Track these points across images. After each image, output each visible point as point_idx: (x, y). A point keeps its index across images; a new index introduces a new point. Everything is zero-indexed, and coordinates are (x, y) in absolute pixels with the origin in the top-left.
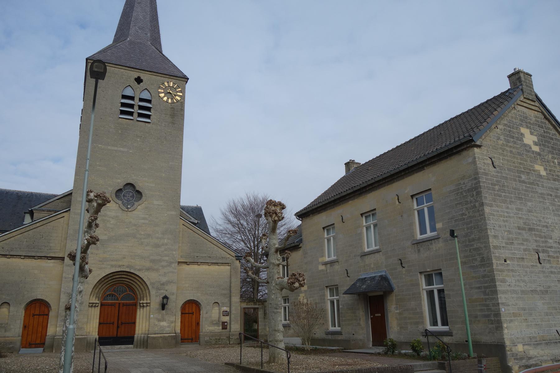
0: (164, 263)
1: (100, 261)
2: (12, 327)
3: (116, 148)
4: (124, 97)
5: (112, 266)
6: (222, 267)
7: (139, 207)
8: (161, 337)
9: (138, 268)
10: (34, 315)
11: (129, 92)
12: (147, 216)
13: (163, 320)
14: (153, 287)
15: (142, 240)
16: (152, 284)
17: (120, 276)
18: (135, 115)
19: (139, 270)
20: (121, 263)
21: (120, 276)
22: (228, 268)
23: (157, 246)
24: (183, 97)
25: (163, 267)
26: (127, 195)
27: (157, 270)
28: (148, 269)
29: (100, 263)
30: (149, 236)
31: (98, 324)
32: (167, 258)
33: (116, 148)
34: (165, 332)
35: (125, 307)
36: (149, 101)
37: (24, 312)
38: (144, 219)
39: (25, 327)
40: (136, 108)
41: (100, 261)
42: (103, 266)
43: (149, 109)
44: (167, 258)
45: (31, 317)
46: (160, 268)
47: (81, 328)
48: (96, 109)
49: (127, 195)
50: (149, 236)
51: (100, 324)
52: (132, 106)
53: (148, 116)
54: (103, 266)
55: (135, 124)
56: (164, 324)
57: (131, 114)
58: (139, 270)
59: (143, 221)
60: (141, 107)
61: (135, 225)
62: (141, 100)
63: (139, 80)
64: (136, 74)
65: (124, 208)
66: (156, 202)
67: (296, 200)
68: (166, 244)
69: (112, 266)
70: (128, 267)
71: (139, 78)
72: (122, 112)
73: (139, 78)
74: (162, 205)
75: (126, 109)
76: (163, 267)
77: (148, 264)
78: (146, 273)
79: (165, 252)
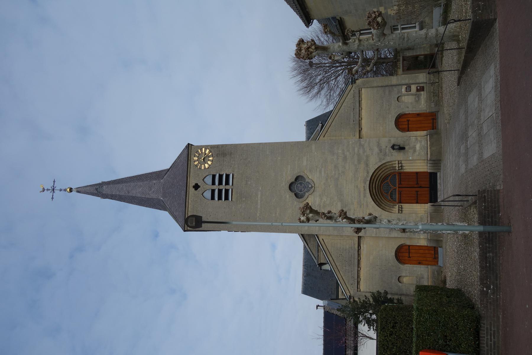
0: (361, 152)
1: (361, 207)
2: (419, 273)
3: (259, 201)
4: (213, 198)
5: (365, 196)
6: (363, 96)
7: (310, 177)
8: (430, 148)
9: (366, 174)
10: (409, 257)
11: (208, 194)
12: (318, 170)
16: (380, 161)
17: (374, 189)
18: (227, 187)
19: (368, 173)
20: (362, 189)
21: (374, 189)
22: (363, 90)
23: (345, 159)
24: (206, 147)
25: (364, 151)
27: (367, 157)
28: (367, 165)
29: (362, 206)
30: (335, 167)
31: (418, 205)
32: (356, 149)
33: (259, 201)
35: (402, 183)
36: (214, 177)
38: (320, 172)
39: (420, 263)
40: (221, 187)
41: (361, 207)
42: (365, 204)
43: (221, 176)
44: (356, 149)
46: (365, 154)
47: (421, 218)
52: (220, 191)
53: (227, 176)
54: (365, 204)
55: (236, 186)
56: (418, 147)
57: (227, 191)
58: (368, 173)
59: (323, 173)
60: (220, 183)
61: (327, 180)
62: (213, 183)
63: (196, 187)
64: (192, 190)
65: (312, 190)
66: (305, 163)
69: (365, 196)
71: (194, 187)
72: (227, 198)
73: (194, 187)
76: (364, 151)
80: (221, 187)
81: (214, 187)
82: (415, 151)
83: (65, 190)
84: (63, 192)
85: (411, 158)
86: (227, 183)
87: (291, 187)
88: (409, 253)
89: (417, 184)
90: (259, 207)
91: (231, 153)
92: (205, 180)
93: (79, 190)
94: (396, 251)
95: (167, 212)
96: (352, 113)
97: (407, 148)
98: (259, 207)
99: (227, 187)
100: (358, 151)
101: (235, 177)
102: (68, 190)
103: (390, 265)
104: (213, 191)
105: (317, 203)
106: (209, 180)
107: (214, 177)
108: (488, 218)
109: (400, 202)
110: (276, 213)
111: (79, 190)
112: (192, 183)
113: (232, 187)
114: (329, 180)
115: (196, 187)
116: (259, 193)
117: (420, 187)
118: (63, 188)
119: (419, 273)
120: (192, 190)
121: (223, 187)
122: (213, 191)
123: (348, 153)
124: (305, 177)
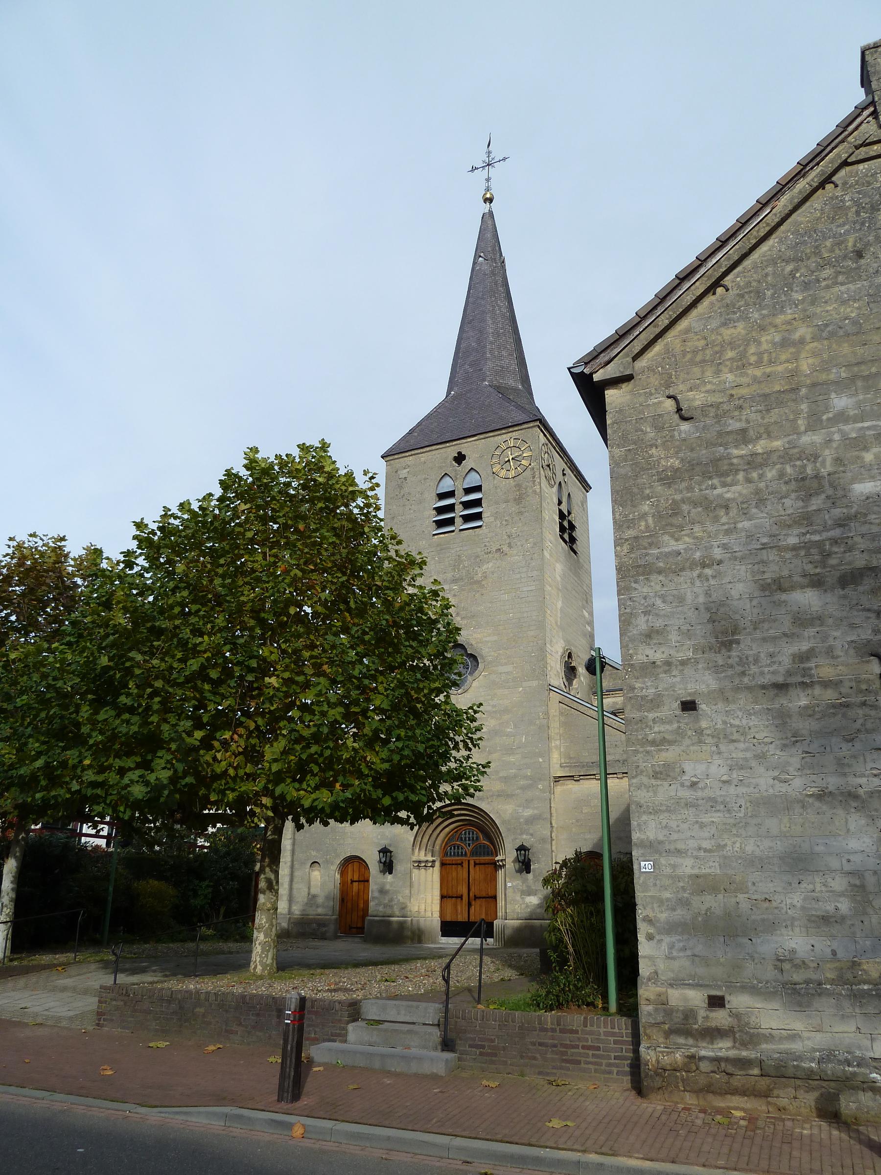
7: (475, 684)
11: (447, 485)
18: (458, 521)
21: (459, 812)
35: (477, 867)
40: (459, 508)
43: (478, 503)
51: (443, 897)
57: (451, 522)
60: (467, 505)
64: (451, 451)
71: (460, 453)
73: (460, 453)
80: (459, 508)
81: (459, 492)
83: (488, 189)
84: (484, 185)
85: (509, 884)
86: (467, 519)
88: (359, 881)
89: (476, 898)
93: (488, 219)
95: (538, 403)
99: (458, 521)
102: (488, 196)
104: (451, 494)
106: (473, 480)
107: (478, 489)
108: (601, 1065)
109: (443, 864)
111: (488, 219)
112: (465, 447)
113: (457, 530)
115: (460, 458)
117: (470, 905)
118: (492, 184)
120: (451, 451)
121: (460, 511)
122: (451, 494)
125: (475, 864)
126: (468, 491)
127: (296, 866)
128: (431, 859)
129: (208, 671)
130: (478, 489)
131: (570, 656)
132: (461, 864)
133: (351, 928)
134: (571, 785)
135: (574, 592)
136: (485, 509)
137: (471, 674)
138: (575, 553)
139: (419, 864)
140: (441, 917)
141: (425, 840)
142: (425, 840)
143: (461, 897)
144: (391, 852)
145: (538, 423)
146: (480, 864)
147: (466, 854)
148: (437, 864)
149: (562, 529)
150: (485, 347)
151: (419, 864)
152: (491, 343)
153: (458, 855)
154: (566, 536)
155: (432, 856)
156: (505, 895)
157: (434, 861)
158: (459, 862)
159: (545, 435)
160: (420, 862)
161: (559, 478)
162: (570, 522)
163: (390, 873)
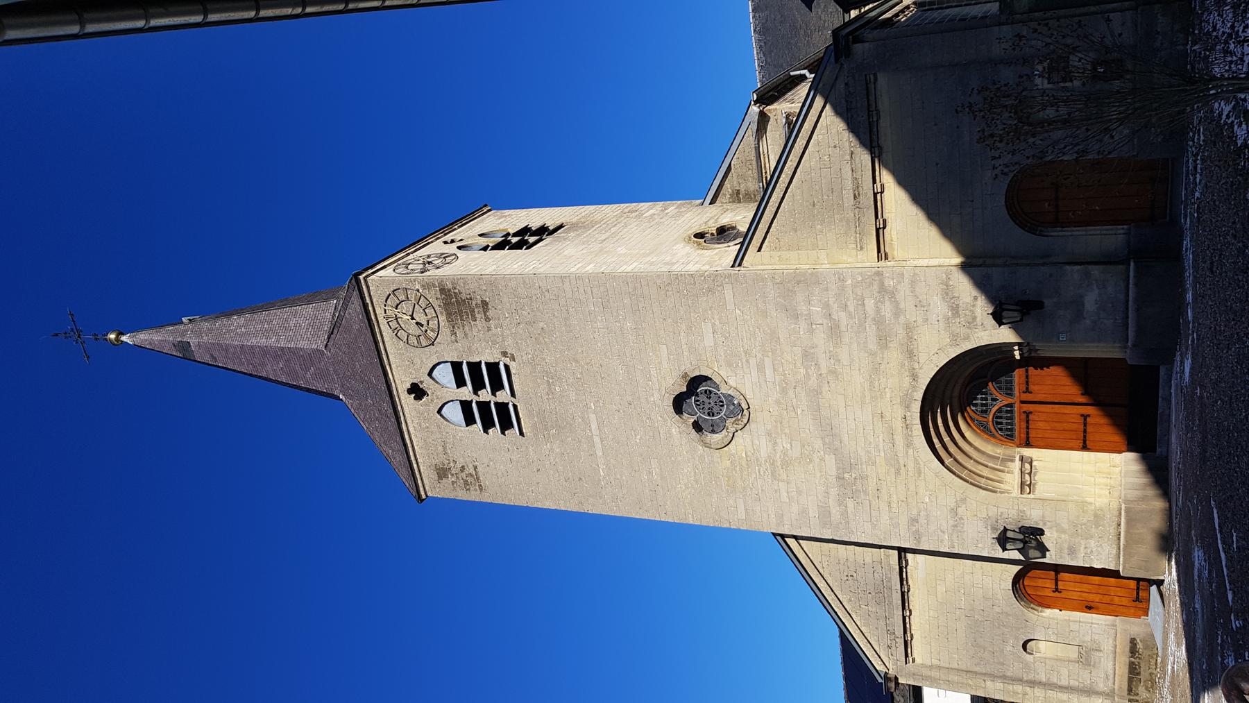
0: (887, 310)
1: (898, 472)
2: (1088, 638)
3: (597, 439)
5: (909, 444)
6: (884, 104)
7: (731, 382)
8: (1137, 310)
9: (907, 381)
10: (1057, 590)
12: (753, 361)
13: (1077, 305)
14: (967, 338)
15: (824, 371)
16: (955, 339)
19: (915, 377)
20: (899, 424)
22: (883, 81)
23: (834, 331)
25: (898, 312)
26: (707, 406)
27: (910, 328)
28: (911, 355)
29: (903, 471)
30: (808, 355)
31: (1086, 453)
32: (870, 303)
33: (597, 439)
34: (1122, 297)
35: (1032, 387)
37: (1048, 612)
38: (761, 368)
39: (1089, 608)
41: (898, 472)
42: (911, 465)
44: (870, 303)
45: (1063, 595)
46: (902, 319)
47: (1096, 516)
48: (558, 223)
49: (707, 406)
50: (808, 355)
51: (1085, 448)
54: (911, 465)
55: (525, 393)
56: (1091, 301)
58: (915, 377)
59: (769, 372)
61: (784, 391)
66: (709, 341)
67: (512, 231)
68: (827, 306)
69: (909, 444)
70: (908, 407)
71: (410, 391)
73: (410, 391)
74: (713, 325)
75: (500, 418)
76: (898, 312)
77: (894, 355)
78: (923, 358)
79: (851, 308)
82: (1079, 315)
87: (679, 404)
90: (599, 453)
91: (485, 304)
92: (435, 373)
94: (1009, 207)
96: (847, 170)
97: (1047, 302)
98: (599, 453)
100: (878, 310)
101: (513, 371)
103: (997, 610)
105: (764, 453)
109: (1028, 444)
110: (650, 473)
112: (401, 383)
114: (791, 393)
115: (417, 391)
116: (593, 416)
119: (1088, 638)
120: (407, 402)
122: (466, 405)
123: (843, 315)
124: (717, 379)
125: (1027, 391)
126: (460, 382)
127: (1031, 677)
128: (1018, 463)
129: (1097, 291)
130: (456, 367)
131: (700, 235)
132: (1028, 414)
133: (1137, 599)
134: (890, 233)
135: (613, 230)
136: (485, 356)
137: (717, 388)
138: (561, 226)
139: (1026, 486)
140: (1120, 452)
141: (986, 472)
142: (986, 472)
143: (1085, 417)
144: (1005, 530)
145: (361, 277)
146: (1027, 383)
147: (1011, 405)
148: (1027, 452)
149: (518, 246)
150: (282, 349)
151: (1026, 486)
152: (278, 341)
153: (1011, 418)
154: (532, 239)
155: (1013, 461)
156: (871, 131)
157: (1022, 459)
158: (1024, 416)
159: (384, 267)
160: (1022, 484)
161: (452, 248)
162: (515, 235)
163: (1042, 532)
